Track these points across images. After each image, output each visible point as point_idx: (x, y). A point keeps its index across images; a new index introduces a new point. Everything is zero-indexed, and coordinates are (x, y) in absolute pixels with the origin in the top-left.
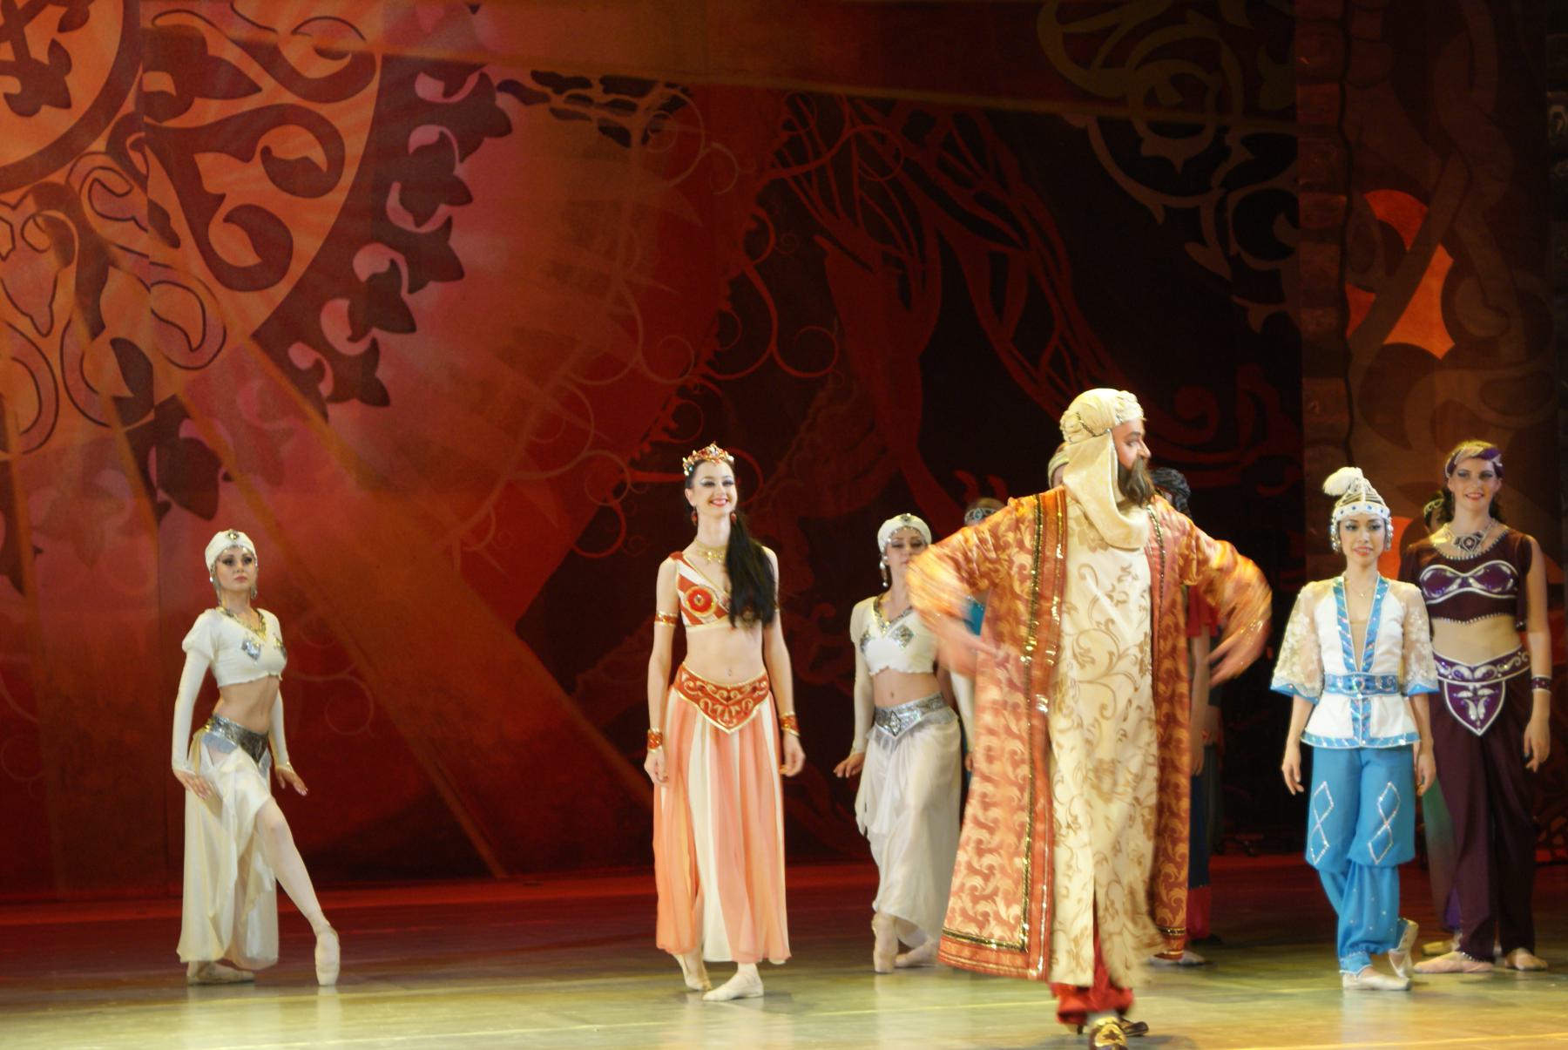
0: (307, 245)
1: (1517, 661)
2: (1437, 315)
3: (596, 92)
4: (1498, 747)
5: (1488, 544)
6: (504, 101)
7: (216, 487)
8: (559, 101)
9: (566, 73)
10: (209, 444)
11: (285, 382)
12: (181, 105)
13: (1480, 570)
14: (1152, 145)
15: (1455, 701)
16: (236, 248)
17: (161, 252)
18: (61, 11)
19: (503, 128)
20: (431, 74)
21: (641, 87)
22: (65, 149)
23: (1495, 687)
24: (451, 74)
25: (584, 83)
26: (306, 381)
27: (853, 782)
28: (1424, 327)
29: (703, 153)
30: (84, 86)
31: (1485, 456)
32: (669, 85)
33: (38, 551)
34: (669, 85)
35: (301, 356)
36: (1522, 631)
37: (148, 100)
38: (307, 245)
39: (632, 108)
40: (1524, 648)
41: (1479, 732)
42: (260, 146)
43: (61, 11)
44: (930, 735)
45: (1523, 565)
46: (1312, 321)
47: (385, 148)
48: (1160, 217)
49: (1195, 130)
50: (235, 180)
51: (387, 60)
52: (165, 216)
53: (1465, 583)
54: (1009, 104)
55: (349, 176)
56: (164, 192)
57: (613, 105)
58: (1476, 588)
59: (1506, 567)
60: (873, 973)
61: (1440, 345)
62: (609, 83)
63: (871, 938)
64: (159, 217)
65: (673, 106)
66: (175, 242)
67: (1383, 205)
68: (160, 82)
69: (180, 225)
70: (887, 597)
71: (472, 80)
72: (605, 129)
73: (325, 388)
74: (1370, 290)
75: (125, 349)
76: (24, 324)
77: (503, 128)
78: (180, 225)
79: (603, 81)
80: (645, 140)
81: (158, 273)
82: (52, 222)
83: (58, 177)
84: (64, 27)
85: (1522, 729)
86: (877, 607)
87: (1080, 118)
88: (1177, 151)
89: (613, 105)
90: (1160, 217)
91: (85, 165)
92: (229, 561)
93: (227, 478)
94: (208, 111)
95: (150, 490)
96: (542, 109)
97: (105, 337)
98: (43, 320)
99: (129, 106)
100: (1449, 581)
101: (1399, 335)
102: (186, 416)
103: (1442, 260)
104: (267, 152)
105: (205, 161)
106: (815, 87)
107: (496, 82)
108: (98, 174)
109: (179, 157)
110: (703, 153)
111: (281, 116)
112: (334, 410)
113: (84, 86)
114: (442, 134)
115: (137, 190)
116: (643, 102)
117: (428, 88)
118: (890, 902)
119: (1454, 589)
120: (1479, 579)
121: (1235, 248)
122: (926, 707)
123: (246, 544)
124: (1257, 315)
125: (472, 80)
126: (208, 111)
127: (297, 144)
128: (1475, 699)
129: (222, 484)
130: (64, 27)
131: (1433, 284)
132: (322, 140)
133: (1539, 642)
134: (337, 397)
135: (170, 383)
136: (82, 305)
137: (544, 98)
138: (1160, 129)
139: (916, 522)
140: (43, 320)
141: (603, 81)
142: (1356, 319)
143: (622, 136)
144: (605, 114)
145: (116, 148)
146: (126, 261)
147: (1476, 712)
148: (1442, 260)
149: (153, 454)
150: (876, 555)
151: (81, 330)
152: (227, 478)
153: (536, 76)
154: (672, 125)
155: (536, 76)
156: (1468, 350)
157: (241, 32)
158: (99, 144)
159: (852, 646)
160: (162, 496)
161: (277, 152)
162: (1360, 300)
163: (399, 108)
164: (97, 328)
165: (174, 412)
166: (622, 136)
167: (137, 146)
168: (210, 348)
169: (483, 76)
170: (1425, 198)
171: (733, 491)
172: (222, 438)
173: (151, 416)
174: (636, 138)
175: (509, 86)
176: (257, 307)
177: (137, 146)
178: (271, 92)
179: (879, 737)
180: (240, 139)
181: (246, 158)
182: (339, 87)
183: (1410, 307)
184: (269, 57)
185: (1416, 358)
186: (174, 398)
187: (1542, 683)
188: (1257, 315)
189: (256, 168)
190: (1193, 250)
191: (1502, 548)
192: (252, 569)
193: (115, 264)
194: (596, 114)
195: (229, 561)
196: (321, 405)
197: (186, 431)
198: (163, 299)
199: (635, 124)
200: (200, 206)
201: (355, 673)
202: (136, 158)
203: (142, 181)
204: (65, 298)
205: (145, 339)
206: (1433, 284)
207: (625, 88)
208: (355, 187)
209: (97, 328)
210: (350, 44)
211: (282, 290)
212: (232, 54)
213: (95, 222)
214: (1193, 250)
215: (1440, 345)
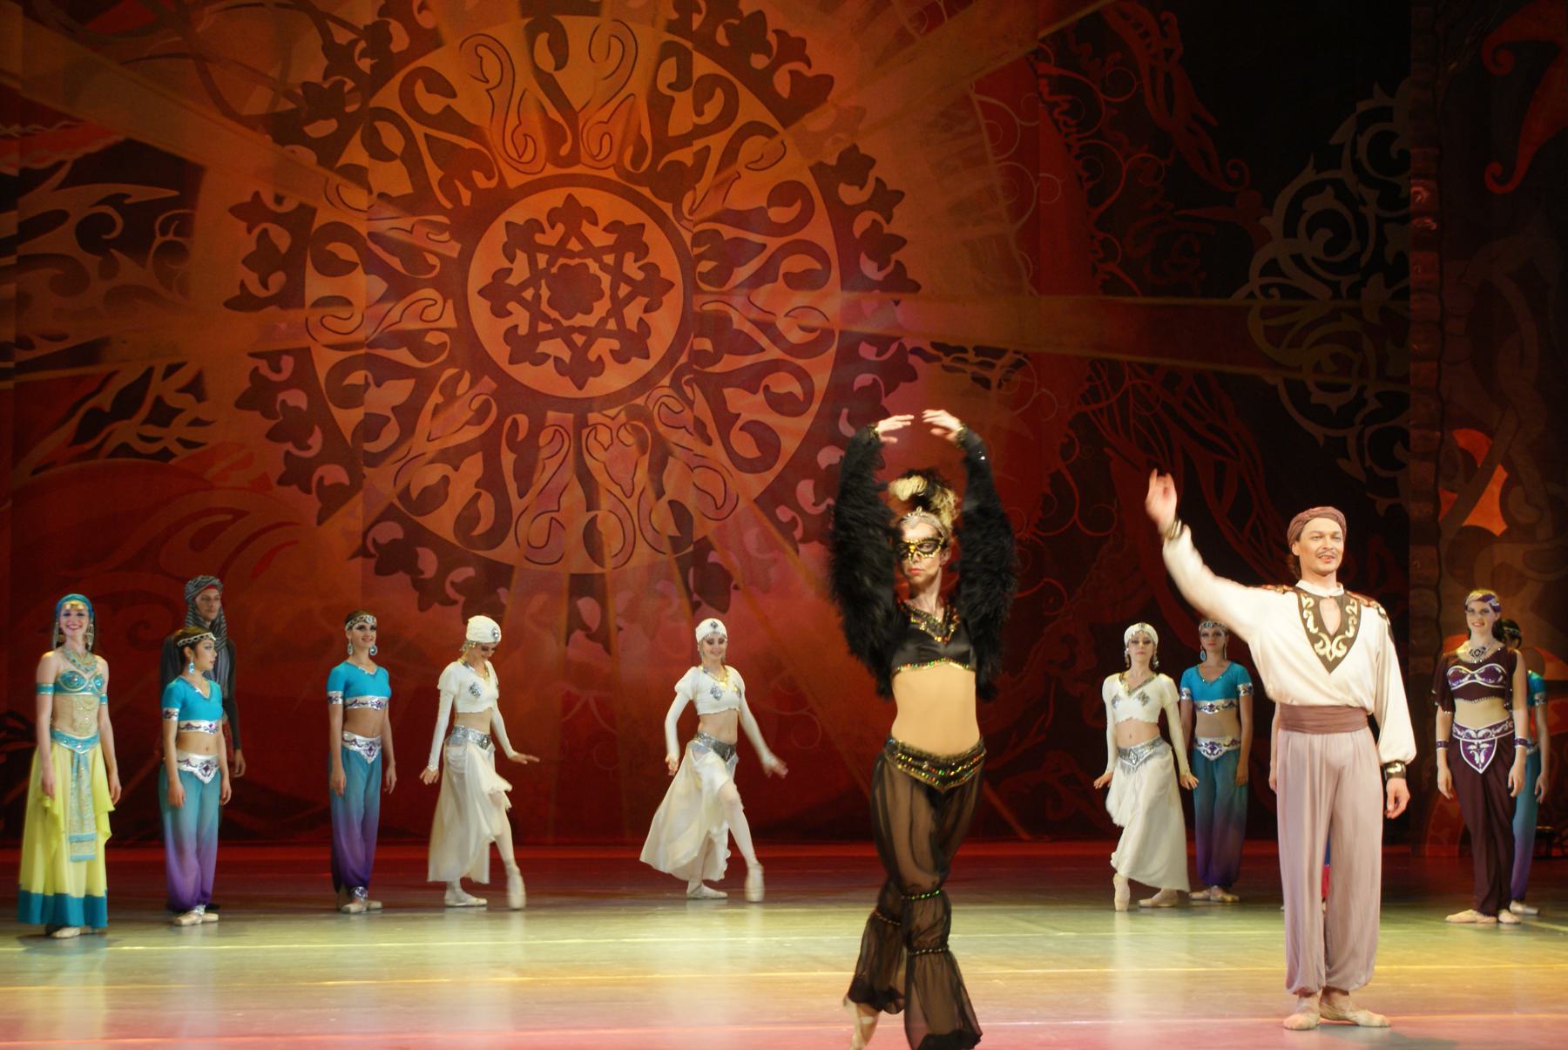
0: (790, 445)
1: (1506, 726)
2: (1497, 509)
3: (970, 356)
4: (1492, 778)
5: (1489, 653)
6: (913, 360)
7: (729, 593)
8: (947, 361)
9: (952, 344)
10: (726, 567)
11: (773, 529)
12: (715, 359)
13: (1482, 669)
14: (1318, 397)
15: (1467, 752)
16: (746, 447)
17: (699, 447)
18: (646, 300)
19: (912, 376)
20: (871, 344)
21: (999, 353)
22: (645, 383)
23: (1492, 742)
24: (881, 342)
25: (963, 350)
26: (786, 529)
27: (1106, 789)
28: (1488, 515)
29: (1035, 395)
30: (659, 344)
31: (1485, 599)
32: (1016, 352)
33: (620, 629)
34: (1016, 352)
35: (784, 514)
36: (1509, 708)
37: (698, 356)
38: (790, 445)
39: (992, 366)
40: (1511, 719)
41: (1481, 771)
42: (764, 383)
43: (646, 300)
44: (1155, 763)
45: (1511, 668)
46: (1417, 510)
47: (839, 392)
48: (1321, 441)
49: (1343, 388)
50: (746, 405)
51: (841, 333)
52: (704, 425)
53: (1473, 677)
54: (1228, 369)
55: (815, 407)
56: (702, 409)
57: (980, 364)
58: (1479, 680)
59: (1499, 668)
60: (1114, 909)
61: (1498, 527)
62: (979, 350)
63: (1113, 890)
64: (700, 427)
65: (1018, 365)
66: (709, 442)
67: (1464, 438)
68: (707, 345)
69: (712, 430)
70: (1127, 674)
71: (894, 346)
72: (977, 379)
73: (798, 534)
74: (1453, 491)
75: (677, 508)
76: (616, 490)
77: (912, 376)
78: (712, 430)
79: (975, 349)
80: (1000, 386)
81: (697, 461)
82: (635, 428)
83: (640, 401)
84: (646, 310)
85: (1508, 770)
86: (1121, 679)
87: (1273, 379)
88: (1334, 401)
89: (980, 364)
90: (1321, 441)
91: (657, 393)
92: (711, 642)
93: (736, 588)
94: (728, 363)
95: (690, 594)
96: (937, 364)
97: (665, 499)
98: (628, 488)
99: (683, 359)
100: (1463, 676)
101: (1472, 520)
102: (712, 548)
103: (1500, 474)
104: (767, 388)
105: (728, 392)
106: (1104, 355)
107: (909, 348)
108: (664, 399)
109: (713, 389)
110: (1035, 395)
111: (774, 366)
112: (801, 547)
113: (659, 344)
114: (791, 72)
115: (687, 410)
116: (999, 363)
117: (867, 352)
118: (1123, 859)
119: (1465, 681)
120: (1481, 675)
121: (1368, 463)
122: (1153, 744)
123: (722, 629)
124: (1382, 505)
125: (894, 346)
126: (728, 363)
127: (786, 385)
128: (1479, 750)
129: (733, 592)
130: (646, 310)
131: (1494, 489)
132: (799, 380)
133: (1520, 715)
134: (804, 540)
135: (704, 528)
136: (652, 480)
137: (939, 359)
138: (1323, 387)
139: (1149, 628)
140: (628, 488)
141: (975, 349)
142: (1445, 509)
143: (986, 383)
144: (975, 369)
145: (676, 384)
146: (677, 451)
147: (1480, 758)
148: (1500, 474)
149: (691, 571)
150: (1122, 646)
151: (650, 494)
152: (736, 588)
153: (934, 345)
154: (1017, 377)
155: (934, 345)
156: (1516, 531)
157: (754, 315)
158: (666, 381)
159: (1103, 706)
160: (696, 597)
161: (774, 389)
162: (1447, 497)
163: (848, 357)
164: (660, 493)
165: (704, 546)
166: (986, 383)
167: (687, 383)
168: (727, 508)
169: (901, 345)
170: (1491, 435)
171: (374, 634)
172: (734, 562)
173: (691, 548)
174: (994, 384)
175: (917, 351)
176: (756, 484)
177: (687, 383)
178: (774, 353)
179: (1123, 766)
180: (752, 380)
181: (754, 392)
182: (810, 349)
183: (1480, 503)
184: (767, 327)
185: (1483, 535)
186: (705, 538)
187: (1523, 742)
188: (1382, 505)
189: (761, 397)
190: (1342, 463)
191: (1496, 657)
192: (724, 646)
193: (671, 454)
194: (970, 369)
195: (711, 642)
196: (794, 544)
197: (713, 557)
198: (699, 476)
199: (994, 376)
200: (726, 420)
201: (811, 710)
202: (687, 389)
203: (691, 404)
204: (642, 475)
205: (691, 502)
206: (1494, 489)
207: (989, 354)
208: (818, 416)
209: (660, 493)
210: (815, 321)
211: (770, 476)
212: (747, 328)
213: (661, 429)
214: (1342, 463)
215: (1498, 527)
